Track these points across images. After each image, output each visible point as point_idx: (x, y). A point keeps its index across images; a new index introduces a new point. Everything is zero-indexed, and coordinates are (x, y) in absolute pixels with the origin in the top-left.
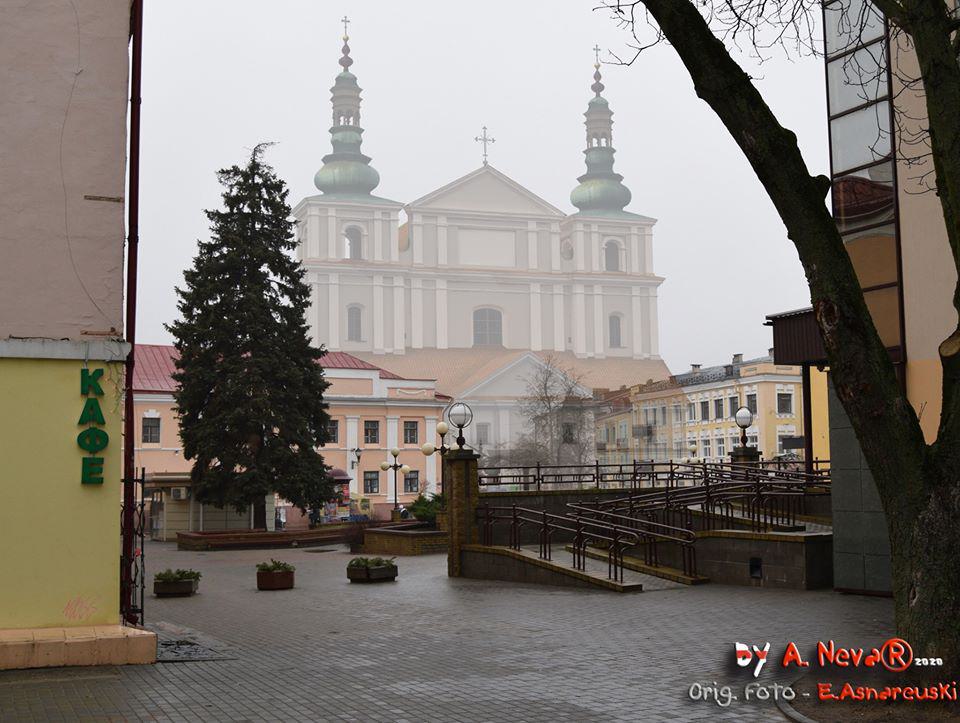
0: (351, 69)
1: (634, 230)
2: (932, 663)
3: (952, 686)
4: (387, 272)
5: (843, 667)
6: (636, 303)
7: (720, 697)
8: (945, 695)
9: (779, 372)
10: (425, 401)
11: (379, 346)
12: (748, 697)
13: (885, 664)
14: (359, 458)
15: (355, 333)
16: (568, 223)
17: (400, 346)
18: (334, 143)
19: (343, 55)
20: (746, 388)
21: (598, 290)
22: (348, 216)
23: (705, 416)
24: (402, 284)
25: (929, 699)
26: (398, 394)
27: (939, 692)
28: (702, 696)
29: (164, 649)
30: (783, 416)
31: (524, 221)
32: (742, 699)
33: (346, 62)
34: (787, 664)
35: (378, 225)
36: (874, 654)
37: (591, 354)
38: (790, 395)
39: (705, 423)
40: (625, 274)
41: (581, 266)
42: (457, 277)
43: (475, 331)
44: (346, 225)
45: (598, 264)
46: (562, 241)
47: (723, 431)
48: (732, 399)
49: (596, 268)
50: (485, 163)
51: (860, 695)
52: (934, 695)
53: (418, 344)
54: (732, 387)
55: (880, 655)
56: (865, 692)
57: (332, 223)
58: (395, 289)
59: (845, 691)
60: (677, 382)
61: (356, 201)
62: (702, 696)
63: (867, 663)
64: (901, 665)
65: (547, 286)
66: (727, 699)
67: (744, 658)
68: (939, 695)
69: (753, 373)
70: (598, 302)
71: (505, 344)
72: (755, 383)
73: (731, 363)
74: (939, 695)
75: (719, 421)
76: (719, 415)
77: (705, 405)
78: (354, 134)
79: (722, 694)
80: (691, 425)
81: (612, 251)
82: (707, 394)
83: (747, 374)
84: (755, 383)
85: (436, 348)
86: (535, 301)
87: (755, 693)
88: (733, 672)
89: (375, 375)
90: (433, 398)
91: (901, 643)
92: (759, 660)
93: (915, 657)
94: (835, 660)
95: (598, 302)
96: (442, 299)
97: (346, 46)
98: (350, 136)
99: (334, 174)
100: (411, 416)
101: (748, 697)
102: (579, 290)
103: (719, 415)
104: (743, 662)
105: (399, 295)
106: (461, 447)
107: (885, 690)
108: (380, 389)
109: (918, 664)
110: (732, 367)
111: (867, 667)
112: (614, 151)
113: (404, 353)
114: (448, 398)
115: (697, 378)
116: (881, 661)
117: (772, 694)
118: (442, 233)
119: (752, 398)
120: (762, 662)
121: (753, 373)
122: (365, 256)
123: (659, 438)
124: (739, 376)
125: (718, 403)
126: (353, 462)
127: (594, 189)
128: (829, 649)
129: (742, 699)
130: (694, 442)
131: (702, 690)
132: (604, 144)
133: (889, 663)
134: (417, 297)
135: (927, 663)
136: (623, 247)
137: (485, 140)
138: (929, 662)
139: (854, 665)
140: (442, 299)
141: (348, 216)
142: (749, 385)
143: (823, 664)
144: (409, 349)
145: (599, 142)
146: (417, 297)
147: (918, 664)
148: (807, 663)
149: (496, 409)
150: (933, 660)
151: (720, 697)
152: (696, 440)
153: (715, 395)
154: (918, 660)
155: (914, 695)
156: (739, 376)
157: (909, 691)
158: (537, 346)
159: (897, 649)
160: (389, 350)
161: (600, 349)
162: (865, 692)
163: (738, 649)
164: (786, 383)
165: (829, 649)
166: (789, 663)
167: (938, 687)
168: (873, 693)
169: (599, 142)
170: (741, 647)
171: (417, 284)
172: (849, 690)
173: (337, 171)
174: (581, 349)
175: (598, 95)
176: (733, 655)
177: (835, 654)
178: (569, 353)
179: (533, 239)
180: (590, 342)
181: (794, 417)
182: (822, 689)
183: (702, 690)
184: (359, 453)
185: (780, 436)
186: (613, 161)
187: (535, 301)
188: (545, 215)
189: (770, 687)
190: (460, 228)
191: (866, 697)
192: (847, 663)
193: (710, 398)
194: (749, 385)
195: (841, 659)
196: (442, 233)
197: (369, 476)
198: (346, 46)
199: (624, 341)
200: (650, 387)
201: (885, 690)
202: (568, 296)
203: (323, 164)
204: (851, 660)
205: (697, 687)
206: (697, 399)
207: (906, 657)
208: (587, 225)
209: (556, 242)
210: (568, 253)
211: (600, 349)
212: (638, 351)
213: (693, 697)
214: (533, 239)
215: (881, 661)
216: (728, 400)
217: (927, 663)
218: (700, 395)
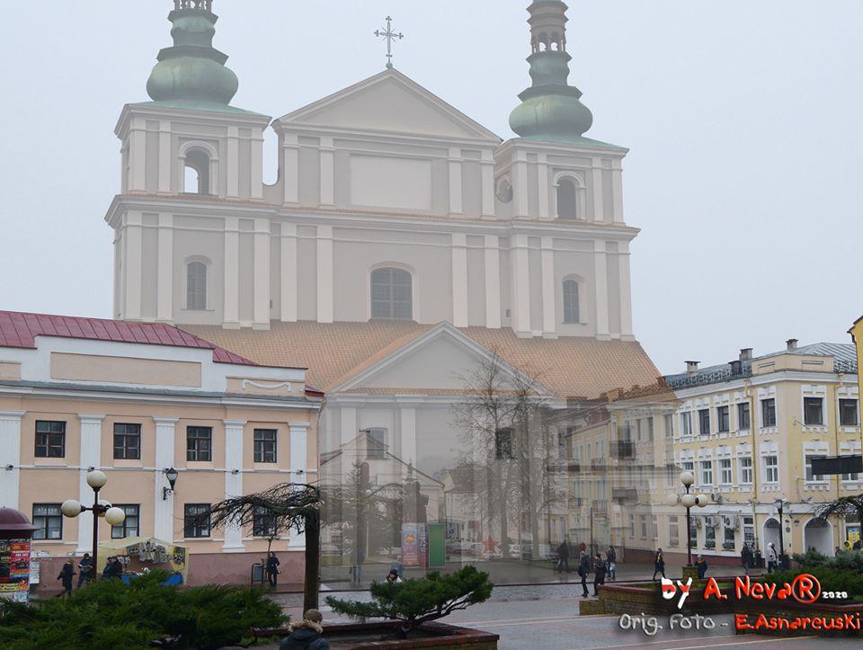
1: (597, 163)
2: (838, 596)
3: (856, 617)
4: (247, 211)
5: (758, 599)
6: (600, 262)
8: (850, 625)
9: (806, 367)
10: (289, 399)
11: (231, 316)
13: (796, 597)
14: (172, 483)
15: (196, 297)
16: (505, 154)
17: (262, 317)
18: (174, 33)
20: (760, 391)
23: (705, 429)
24: (604, 250)
25: (835, 628)
26: (243, 388)
27: (844, 622)
28: (632, 626)
30: (811, 428)
31: (446, 145)
34: (707, 597)
36: (786, 588)
37: (537, 333)
38: (821, 399)
39: (705, 438)
40: (585, 224)
41: (523, 210)
43: (373, 298)
44: (186, 145)
45: (547, 209)
46: (496, 179)
47: (729, 450)
48: (742, 406)
49: (544, 213)
50: (389, 66)
51: (773, 625)
52: (839, 625)
53: (289, 315)
54: (740, 389)
55: (790, 589)
56: (777, 622)
57: (165, 143)
60: (667, 386)
61: (204, 108)
62: (632, 626)
63: (779, 595)
64: (809, 598)
65: (474, 236)
66: (654, 628)
67: (669, 592)
68: (844, 625)
69: (771, 369)
70: (547, 261)
71: (416, 317)
72: (772, 383)
73: (738, 359)
74: (844, 625)
75: (724, 435)
76: (723, 428)
77: (704, 414)
78: (204, 22)
79: (649, 624)
80: (685, 441)
81: (566, 192)
82: (707, 400)
83: (762, 370)
84: (772, 383)
85: (316, 322)
86: (459, 259)
87: (679, 623)
89: (206, 357)
90: (303, 395)
94: (750, 593)
95: (547, 261)
96: (325, 250)
98: (200, 23)
99: (175, 72)
100: (266, 421)
101: (672, 627)
102: (520, 242)
103: (723, 428)
104: (668, 596)
105: (262, 246)
108: (215, 378)
109: (825, 597)
110: (739, 362)
111: (780, 599)
112: (569, 58)
113: (268, 328)
114: (321, 394)
115: (694, 379)
116: (792, 594)
117: (694, 624)
118: (327, 161)
119: (768, 405)
120: (685, 595)
121: (771, 369)
122: (214, 191)
123: (642, 458)
124: (749, 374)
125: (722, 411)
126: (165, 490)
127: (542, 107)
130: (690, 465)
131: (631, 621)
132: (554, 47)
133: (799, 596)
134: (289, 249)
135: (833, 596)
136: (582, 186)
137: (389, 35)
138: (835, 595)
139: (768, 598)
140: (325, 250)
142: (764, 386)
143: (740, 597)
144: (276, 323)
145: (548, 46)
146: (289, 249)
147: (825, 597)
148: (726, 596)
149: (396, 408)
150: (838, 594)
152: (693, 461)
153: (720, 400)
154: (825, 594)
156: (749, 374)
158: (461, 320)
159: (807, 584)
160: (247, 324)
161: (551, 324)
163: (663, 583)
164: (815, 383)
167: (844, 618)
169: (548, 46)
170: (666, 582)
171: (289, 230)
172: (763, 620)
173: (177, 70)
174: (523, 326)
176: (660, 588)
178: (507, 331)
179: (455, 170)
180: (537, 316)
181: (826, 430)
182: (738, 620)
183: (631, 621)
184: (172, 476)
185: (807, 457)
186: (567, 71)
187: (459, 259)
188: (473, 136)
190: (353, 154)
191: (778, 626)
192: (761, 596)
193: (711, 404)
194: (764, 386)
195: (756, 592)
196: (327, 161)
197: (195, 511)
199: (583, 317)
200: (636, 393)
202: (506, 251)
203: (157, 62)
204: (765, 593)
206: (693, 406)
207: (814, 590)
208: (532, 154)
209: (488, 175)
211: (551, 324)
212: (603, 330)
214: (455, 170)
215: (792, 594)
216: (736, 408)
217: (833, 596)
218: (698, 401)
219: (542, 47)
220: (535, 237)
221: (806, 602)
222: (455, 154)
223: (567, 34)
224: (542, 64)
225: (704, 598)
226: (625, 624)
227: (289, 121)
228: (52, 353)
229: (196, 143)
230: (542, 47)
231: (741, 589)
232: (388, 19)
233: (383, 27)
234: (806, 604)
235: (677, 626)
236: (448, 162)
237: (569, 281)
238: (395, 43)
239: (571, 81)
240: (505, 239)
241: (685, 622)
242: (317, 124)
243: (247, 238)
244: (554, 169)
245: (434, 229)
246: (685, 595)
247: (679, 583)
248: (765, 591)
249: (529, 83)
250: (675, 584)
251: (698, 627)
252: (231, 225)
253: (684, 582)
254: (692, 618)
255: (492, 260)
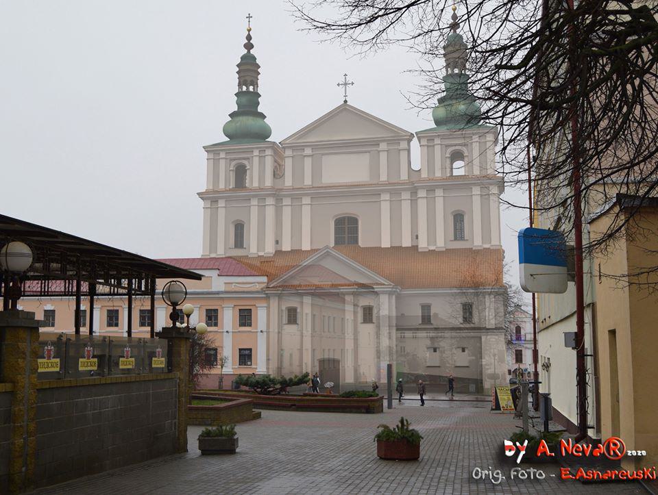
0: (252, 51)
2: (639, 454)
7: (493, 477)
8: (648, 476)
12: (512, 478)
13: (607, 454)
19: (247, 42)
21: (221, 203)
22: (233, 156)
24: (442, 194)
27: (644, 474)
28: (481, 477)
29: (515, 380)
31: (376, 143)
32: (509, 477)
33: (249, 46)
34: (539, 455)
35: (256, 160)
36: (600, 448)
42: (321, 193)
44: (450, 149)
50: (346, 101)
51: (590, 476)
56: (593, 474)
58: (267, 207)
59: (580, 473)
62: (481, 477)
63: (594, 454)
64: (618, 456)
66: (498, 478)
67: (510, 450)
68: (644, 476)
74: (644, 476)
79: (495, 475)
86: (385, 207)
87: (518, 474)
88: (503, 462)
91: (618, 440)
92: (520, 452)
93: (627, 450)
95: (439, 203)
96: (306, 211)
97: (249, 34)
101: (512, 478)
104: (509, 454)
106: (174, 324)
107: (606, 472)
111: (594, 456)
128: (568, 444)
129: (509, 477)
131: (481, 473)
133: (609, 454)
135: (635, 454)
136: (231, 172)
138: (637, 453)
139: (585, 455)
140: (306, 211)
141: (233, 156)
143: (564, 455)
145: (248, 88)
147: (629, 454)
148: (553, 454)
150: (639, 452)
151: (493, 477)
155: (627, 476)
157: (623, 473)
162: (593, 474)
165: (568, 444)
166: (541, 453)
168: (598, 474)
169: (248, 88)
170: (508, 443)
171: (287, 201)
172: (581, 472)
175: (249, 51)
176: (503, 448)
177: (573, 448)
180: (432, 237)
182: (563, 472)
183: (481, 473)
186: (258, 103)
187: (385, 207)
189: (528, 470)
190: (323, 154)
191: (593, 477)
192: (581, 454)
195: (576, 451)
198: (249, 34)
199: (466, 236)
201: (606, 472)
204: (583, 451)
205: (478, 471)
210: (278, 173)
213: (474, 476)
214: (383, 156)
219: (244, 88)
220: (431, 190)
221: (614, 458)
222: (383, 146)
223: (259, 82)
224: (244, 100)
225: (537, 456)
226: (477, 475)
227: (288, 142)
228: (225, 283)
229: (454, 148)
230: (244, 88)
231: (565, 448)
232: (346, 75)
233: (342, 80)
234: (615, 460)
235: (516, 477)
236: (379, 151)
237: (457, 215)
238: (349, 87)
239: (260, 109)
240: (414, 192)
241: (523, 474)
242: (337, 137)
243: (262, 208)
244: (446, 146)
245: (369, 192)
246: (523, 453)
247: (518, 444)
248: (583, 449)
249: (235, 108)
250: (515, 444)
251: (532, 478)
252: (476, 191)
253: (522, 444)
254: (528, 470)
255: (406, 207)
